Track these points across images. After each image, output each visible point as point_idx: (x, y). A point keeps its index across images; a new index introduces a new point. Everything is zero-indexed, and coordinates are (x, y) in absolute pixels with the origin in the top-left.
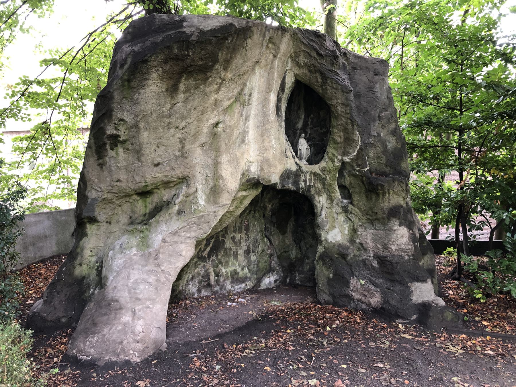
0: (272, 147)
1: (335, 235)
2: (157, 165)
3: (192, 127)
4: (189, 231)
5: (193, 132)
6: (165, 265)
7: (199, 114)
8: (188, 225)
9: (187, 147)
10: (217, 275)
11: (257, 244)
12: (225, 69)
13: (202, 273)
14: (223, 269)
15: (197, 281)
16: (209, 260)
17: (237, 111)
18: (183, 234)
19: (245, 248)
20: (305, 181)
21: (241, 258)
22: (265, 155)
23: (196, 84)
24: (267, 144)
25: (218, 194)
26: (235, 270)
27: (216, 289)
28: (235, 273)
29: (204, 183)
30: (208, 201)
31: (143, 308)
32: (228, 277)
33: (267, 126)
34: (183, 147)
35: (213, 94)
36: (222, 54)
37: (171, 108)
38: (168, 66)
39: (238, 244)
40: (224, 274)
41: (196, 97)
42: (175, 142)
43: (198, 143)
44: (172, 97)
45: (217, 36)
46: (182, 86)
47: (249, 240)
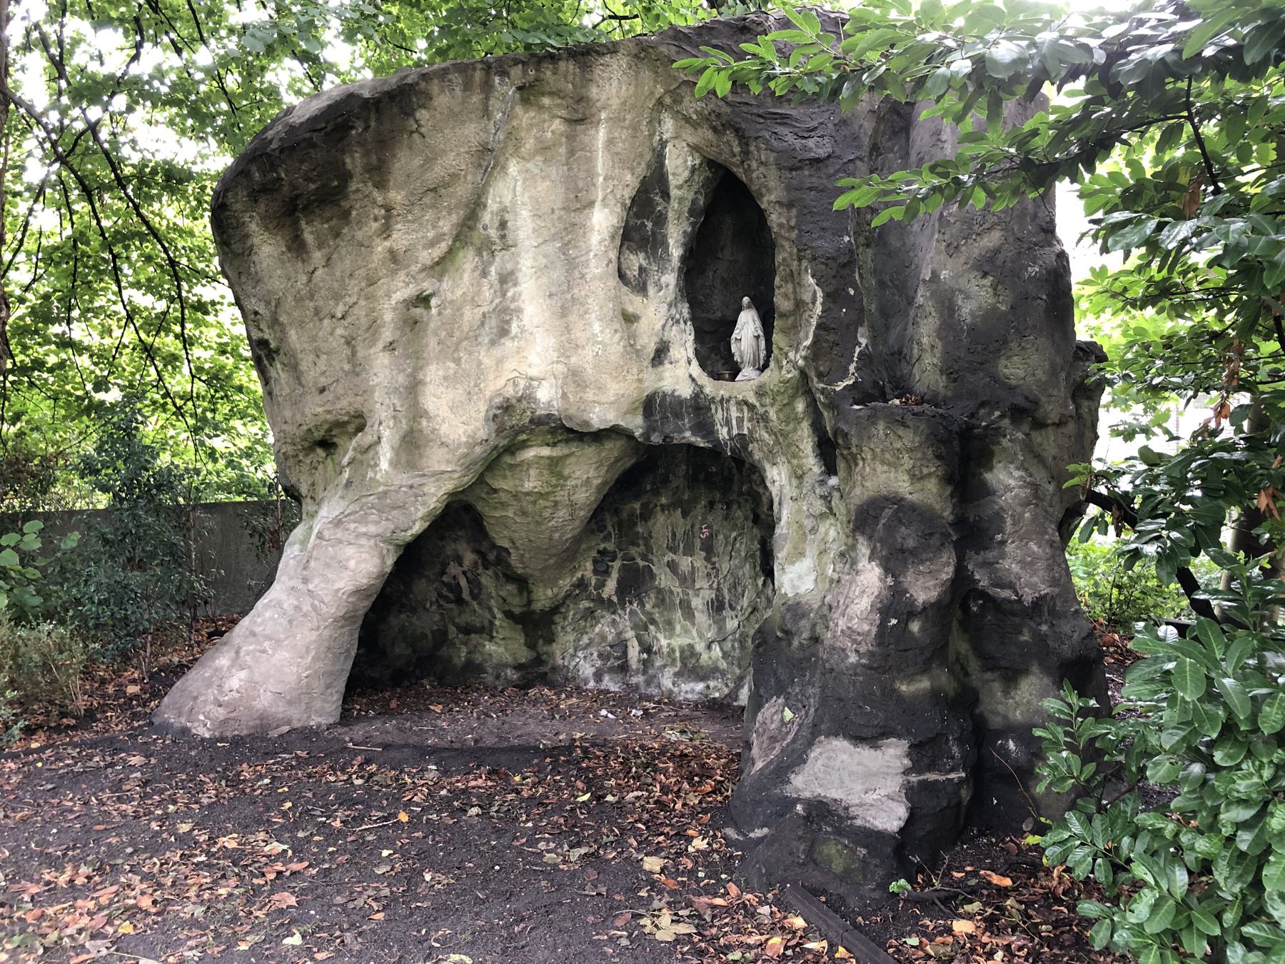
0: (592, 339)
1: (800, 577)
2: (322, 390)
3: (360, 312)
4: (363, 521)
5: (364, 322)
6: (316, 581)
7: (363, 284)
8: (361, 509)
9: (361, 353)
10: (647, 649)
11: (740, 590)
12: (381, 185)
13: (610, 638)
14: (661, 636)
15: (595, 654)
16: (624, 609)
17: (468, 266)
18: (352, 526)
19: (709, 595)
20: (728, 423)
21: (702, 618)
22: (573, 360)
23: (331, 228)
24: (578, 334)
25: (418, 447)
26: (691, 647)
27: (634, 680)
28: (689, 653)
29: (391, 424)
30: (394, 464)
31: (255, 650)
32: (674, 660)
33: (576, 291)
34: (354, 353)
35: (378, 240)
36: (353, 157)
37: (310, 281)
38: (262, 207)
39: (687, 580)
40: (665, 650)
41: (343, 251)
42: (336, 342)
43: (380, 345)
44: (304, 261)
45: (318, 127)
46: (309, 237)
47: (717, 576)
